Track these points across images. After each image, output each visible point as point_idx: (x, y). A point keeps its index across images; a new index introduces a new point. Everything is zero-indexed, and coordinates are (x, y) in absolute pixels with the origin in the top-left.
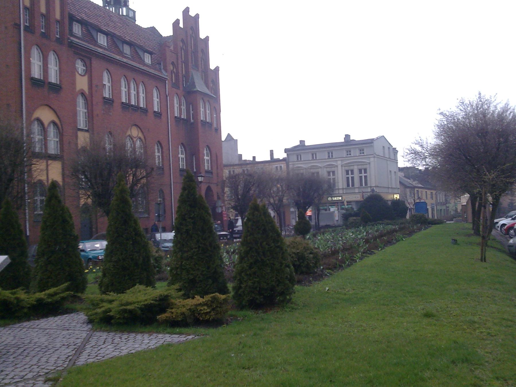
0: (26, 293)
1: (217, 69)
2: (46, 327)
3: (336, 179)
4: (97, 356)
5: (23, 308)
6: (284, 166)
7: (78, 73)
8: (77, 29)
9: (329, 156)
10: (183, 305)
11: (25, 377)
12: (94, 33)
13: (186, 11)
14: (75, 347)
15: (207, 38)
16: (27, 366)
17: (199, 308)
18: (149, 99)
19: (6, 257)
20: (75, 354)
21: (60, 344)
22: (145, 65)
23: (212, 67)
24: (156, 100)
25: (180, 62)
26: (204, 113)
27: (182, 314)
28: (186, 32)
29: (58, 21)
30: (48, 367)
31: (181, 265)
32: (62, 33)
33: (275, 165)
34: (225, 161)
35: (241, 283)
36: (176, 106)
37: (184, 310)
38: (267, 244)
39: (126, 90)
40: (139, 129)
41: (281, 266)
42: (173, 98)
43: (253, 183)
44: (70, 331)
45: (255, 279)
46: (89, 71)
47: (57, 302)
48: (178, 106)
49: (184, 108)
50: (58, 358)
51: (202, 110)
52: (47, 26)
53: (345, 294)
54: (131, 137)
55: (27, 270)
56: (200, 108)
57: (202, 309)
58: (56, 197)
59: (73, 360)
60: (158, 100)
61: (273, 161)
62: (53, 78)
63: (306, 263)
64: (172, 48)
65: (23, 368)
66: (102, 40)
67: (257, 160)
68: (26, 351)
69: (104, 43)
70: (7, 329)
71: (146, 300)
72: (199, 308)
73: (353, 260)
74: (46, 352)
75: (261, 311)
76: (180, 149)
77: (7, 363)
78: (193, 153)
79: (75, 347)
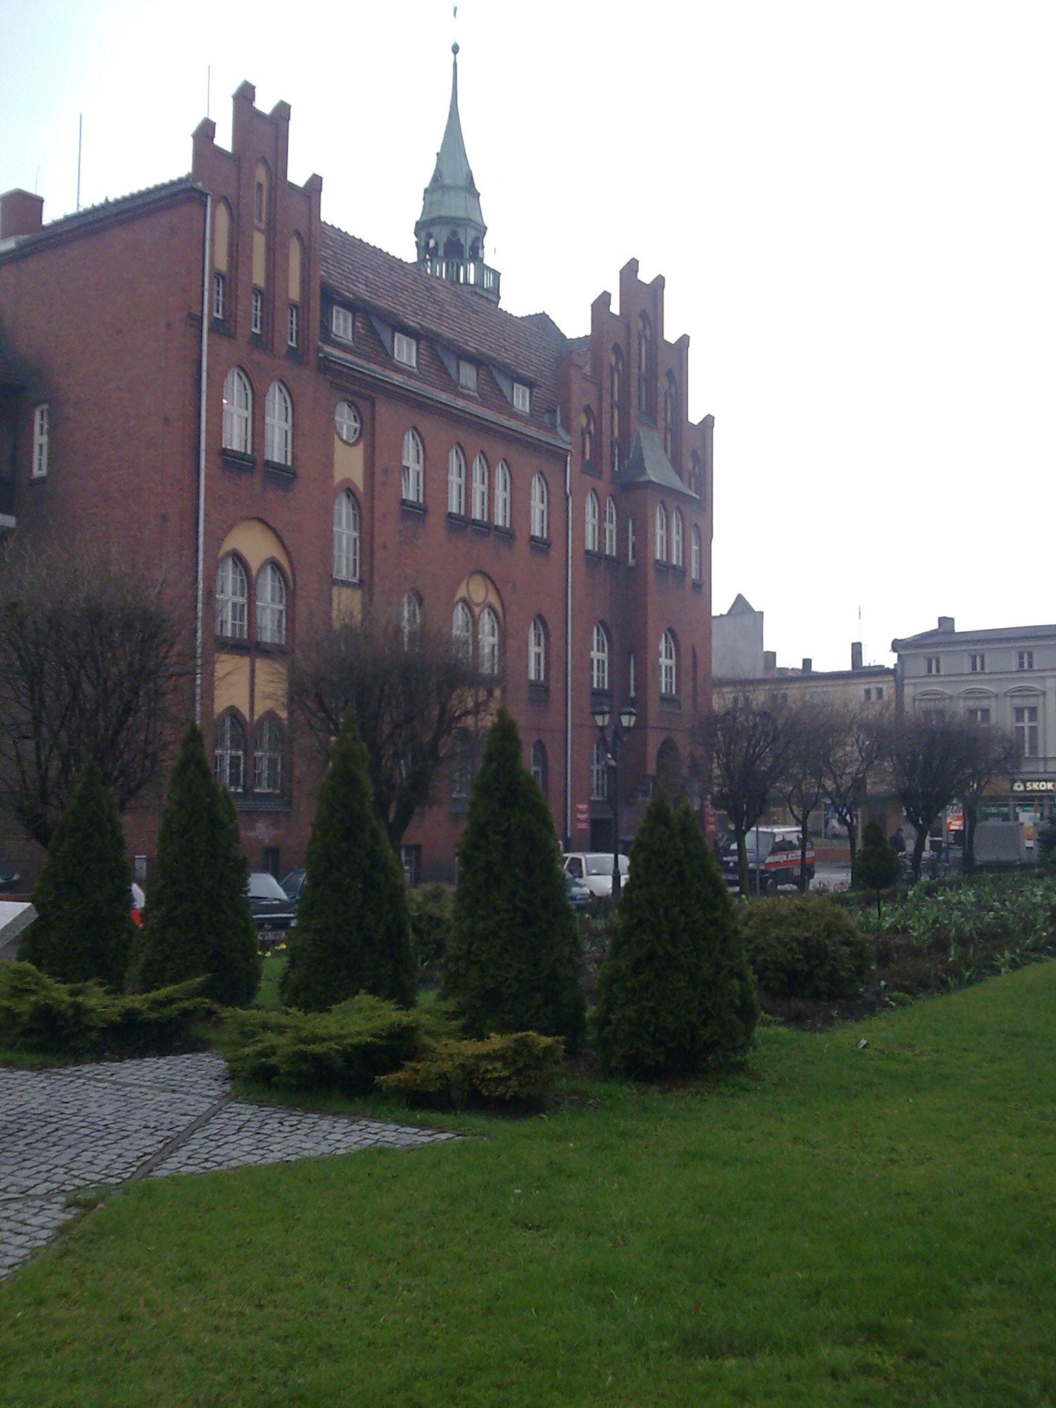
0: (108, 993)
1: (708, 423)
2: (130, 1080)
3: (1040, 730)
4: (206, 1160)
5: (90, 1029)
6: (888, 688)
7: (341, 439)
8: (342, 325)
9: (1021, 665)
10: (452, 1051)
11: (30, 1192)
12: (385, 335)
13: (630, 270)
14: (169, 1133)
15: (684, 341)
16: (43, 1168)
17: (486, 1066)
18: (519, 505)
19: (28, 904)
20: (161, 1151)
21: (140, 1122)
22: (515, 415)
23: (695, 416)
24: (537, 507)
25: (606, 406)
26: (663, 540)
27: (440, 1077)
28: (628, 326)
29: (294, 306)
30: (87, 1176)
31: (469, 951)
32: (303, 333)
33: (858, 690)
34: (719, 669)
35: (610, 1009)
36: (591, 521)
37: (447, 1066)
38: (682, 912)
39: (462, 481)
40: (490, 585)
41: (717, 973)
42: (584, 501)
43: (788, 738)
44: (177, 1096)
45: (644, 1003)
46: (367, 433)
47: (171, 1021)
48: (595, 521)
49: (611, 527)
50: (120, 1156)
51: (659, 532)
52: (267, 321)
53: (907, 1062)
54: (467, 603)
55: (125, 936)
56: (654, 526)
57: (490, 1068)
58: (200, 764)
59: (147, 1164)
60: (544, 507)
61: (859, 671)
62: (276, 451)
63: (828, 968)
64: (587, 370)
65: (34, 1170)
66: (405, 351)
67: (817, 667)
68: (60, 1133)
69: (410, 358)
70: (42, 1077)
71: (359, 1033)
72: (486, 1066)
73: (992, 967)
74: (101, 1138)
75: (654, 1088)
76: (595, 637)
77: (8, 1154)
78: (630, 647)
79: (169, 1133)
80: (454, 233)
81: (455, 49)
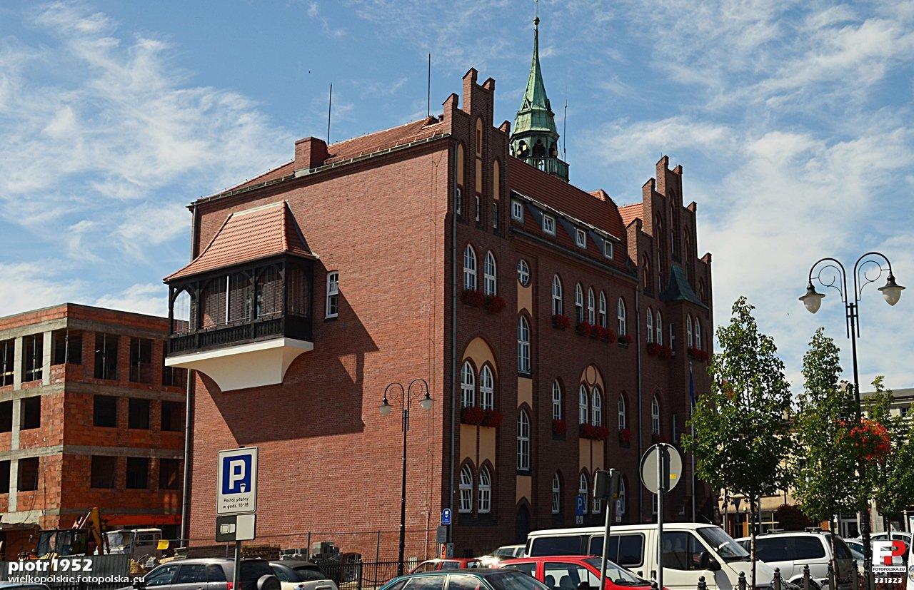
7: (520, 282)
54: (586, 384)
80: (539, 141)
81: (537, 21)
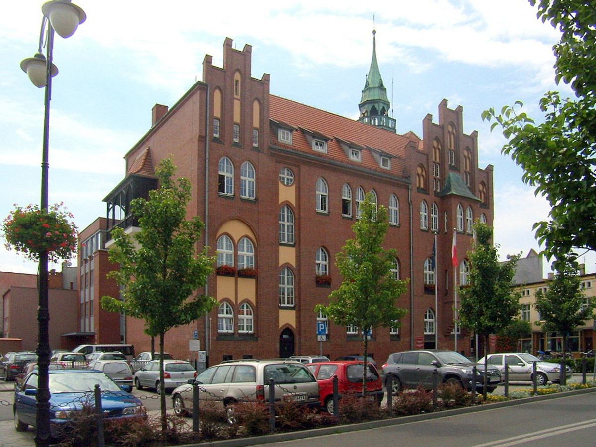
51: (459, 216)
81: (374, 32)
